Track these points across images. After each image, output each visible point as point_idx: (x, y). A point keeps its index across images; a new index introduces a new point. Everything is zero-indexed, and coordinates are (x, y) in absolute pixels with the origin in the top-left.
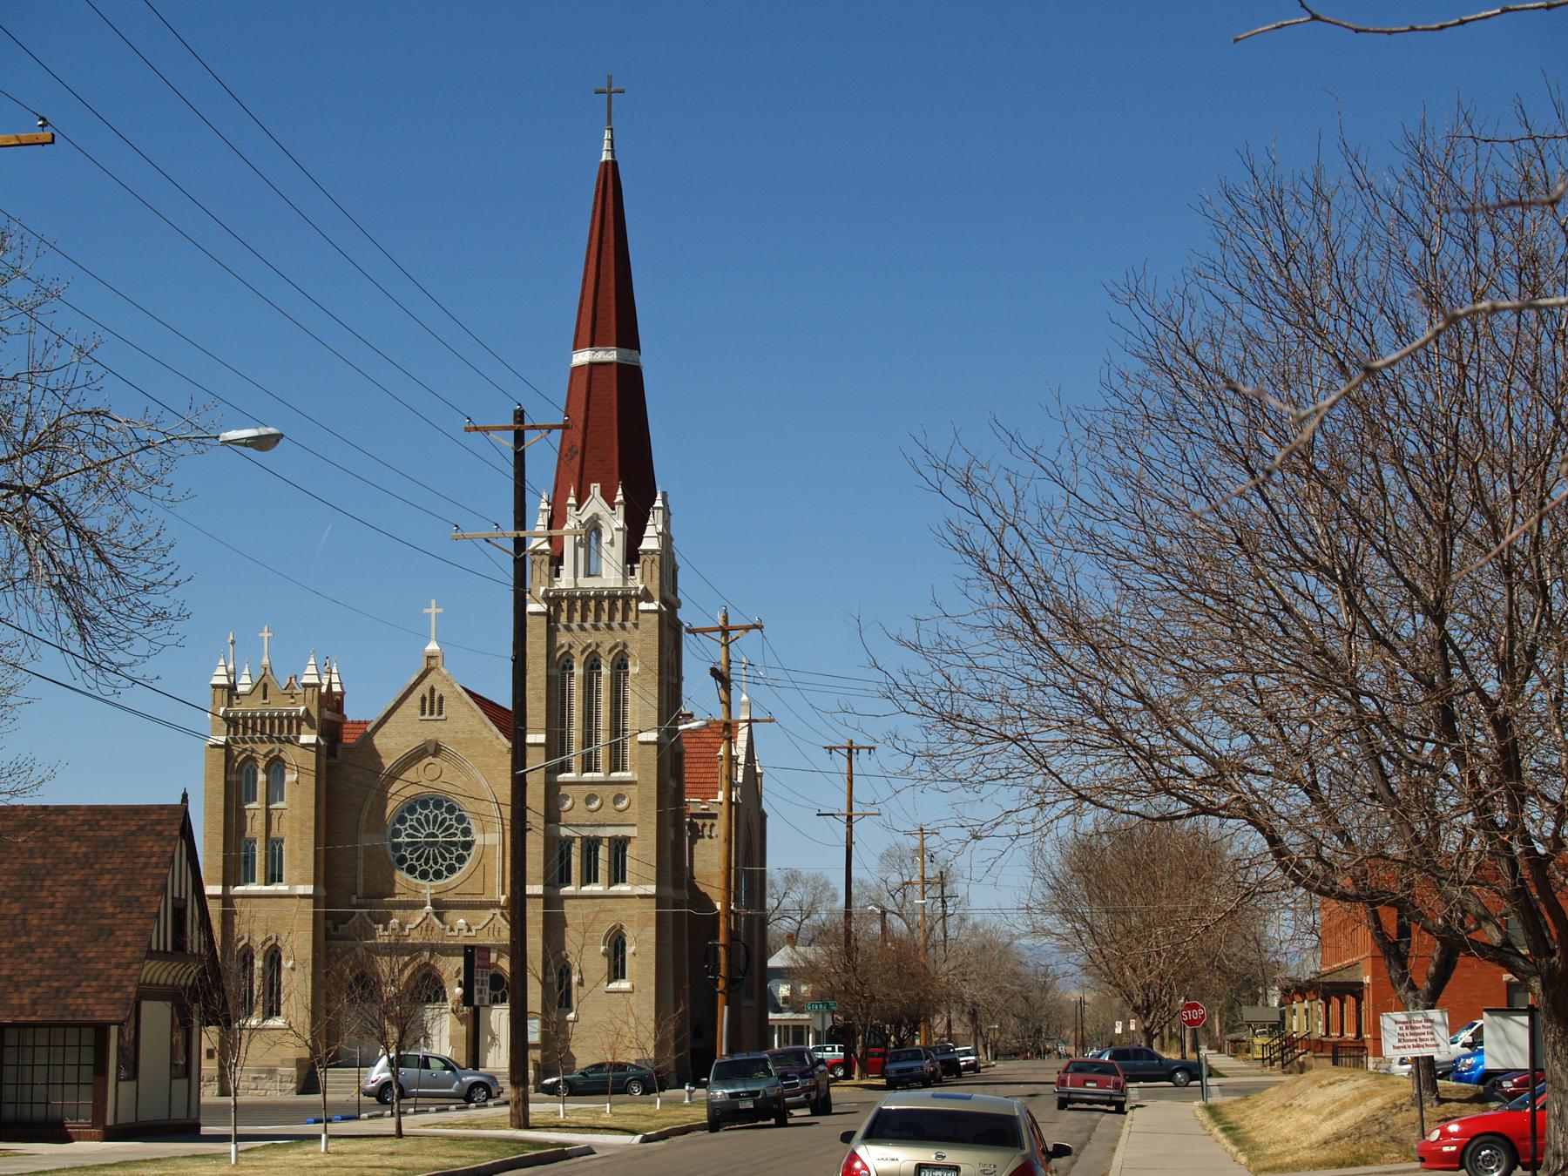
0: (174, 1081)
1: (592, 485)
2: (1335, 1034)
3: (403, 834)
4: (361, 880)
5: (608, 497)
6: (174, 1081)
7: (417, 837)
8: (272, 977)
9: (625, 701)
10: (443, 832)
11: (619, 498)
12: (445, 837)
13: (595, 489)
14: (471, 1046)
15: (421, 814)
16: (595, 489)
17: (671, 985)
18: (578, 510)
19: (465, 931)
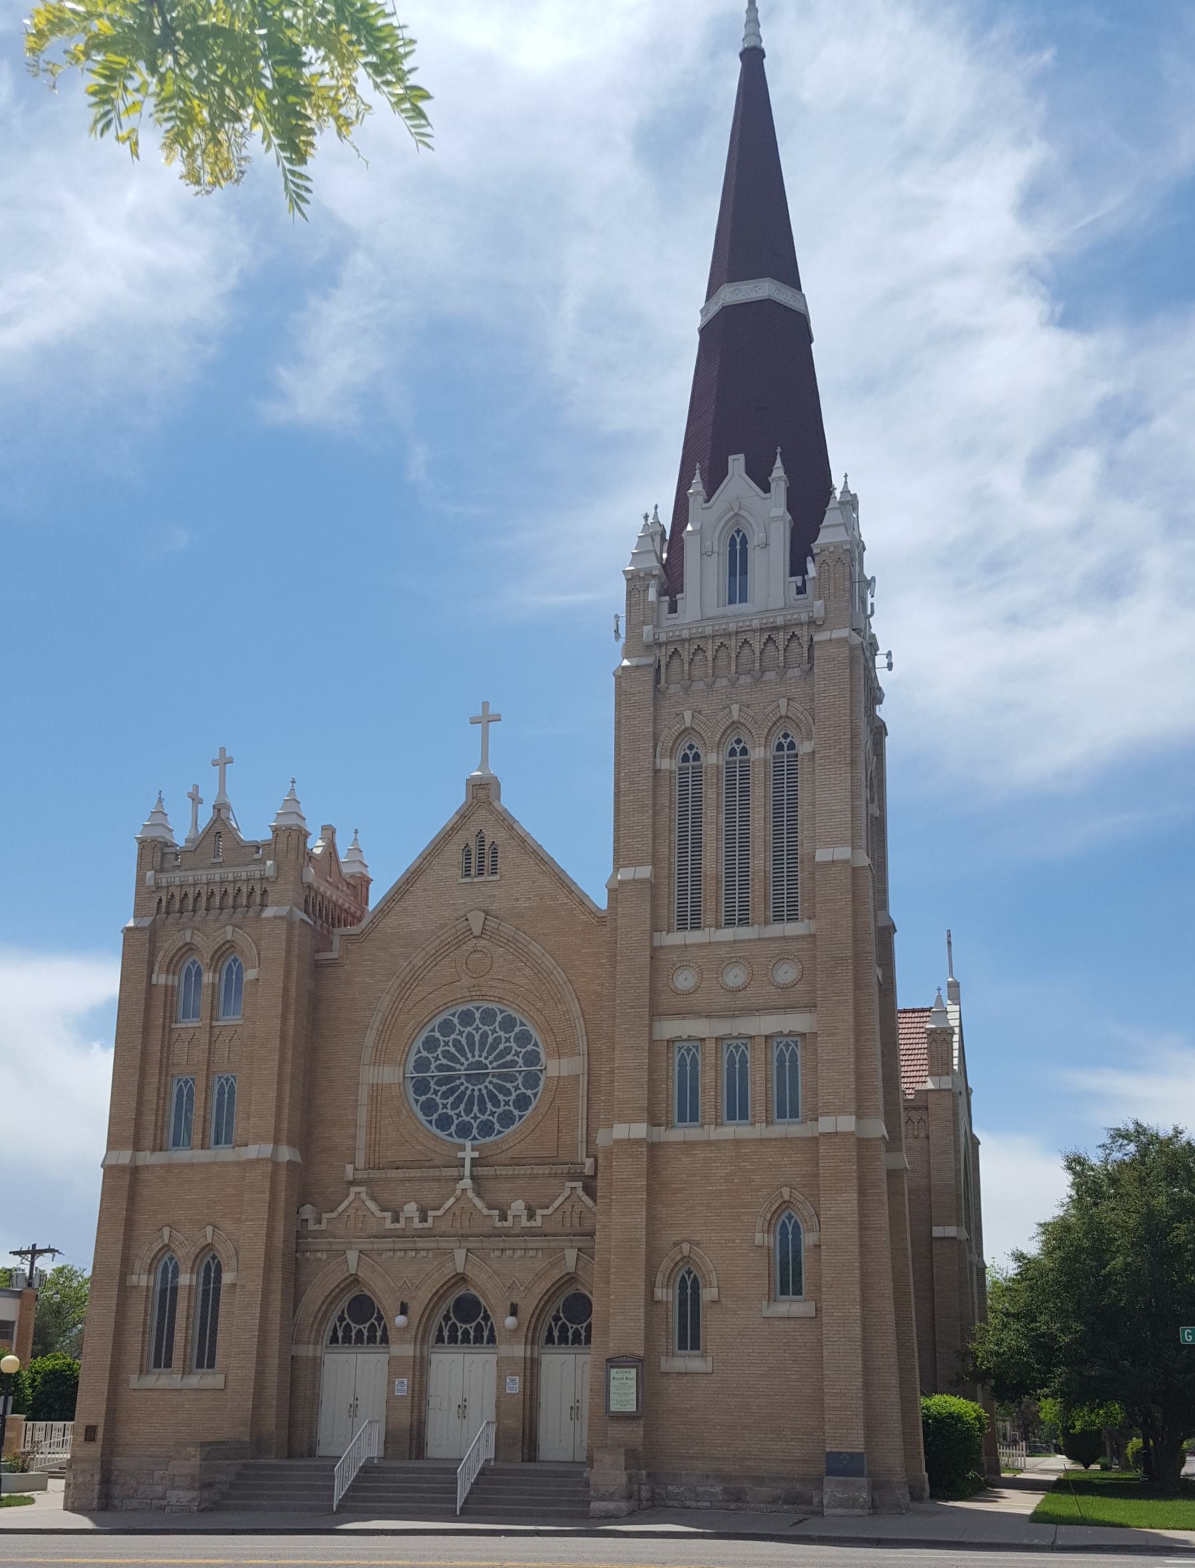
0: (593, 1174)
1: (731, 458)
2: (825, 1347)
3: (433, 1067)
4: (362, 1141)
5: (760, 477)
6: (593, 1174)
7: (455, 1069)
8: (421, 1375)
9: (452, 1176)
10: (495, 1059)
11: (778, 471)
12: (499, 1067)
13: (737, 463)
14: (1068, 1518)
15: (446, 1044)
16: (737, 463)
17: (889, 1306)
18: (707, 501)
19: (524, 1218)
